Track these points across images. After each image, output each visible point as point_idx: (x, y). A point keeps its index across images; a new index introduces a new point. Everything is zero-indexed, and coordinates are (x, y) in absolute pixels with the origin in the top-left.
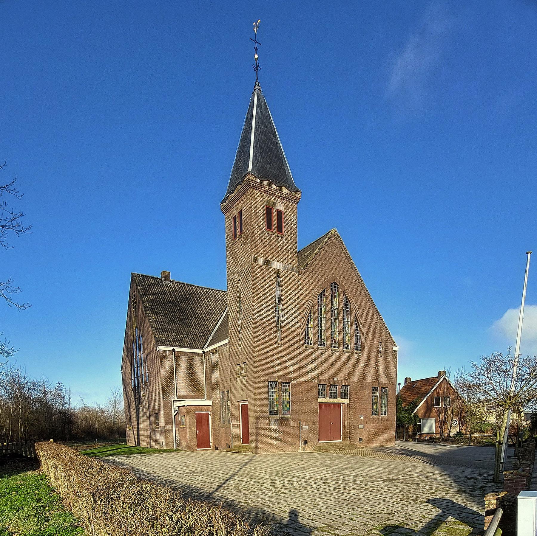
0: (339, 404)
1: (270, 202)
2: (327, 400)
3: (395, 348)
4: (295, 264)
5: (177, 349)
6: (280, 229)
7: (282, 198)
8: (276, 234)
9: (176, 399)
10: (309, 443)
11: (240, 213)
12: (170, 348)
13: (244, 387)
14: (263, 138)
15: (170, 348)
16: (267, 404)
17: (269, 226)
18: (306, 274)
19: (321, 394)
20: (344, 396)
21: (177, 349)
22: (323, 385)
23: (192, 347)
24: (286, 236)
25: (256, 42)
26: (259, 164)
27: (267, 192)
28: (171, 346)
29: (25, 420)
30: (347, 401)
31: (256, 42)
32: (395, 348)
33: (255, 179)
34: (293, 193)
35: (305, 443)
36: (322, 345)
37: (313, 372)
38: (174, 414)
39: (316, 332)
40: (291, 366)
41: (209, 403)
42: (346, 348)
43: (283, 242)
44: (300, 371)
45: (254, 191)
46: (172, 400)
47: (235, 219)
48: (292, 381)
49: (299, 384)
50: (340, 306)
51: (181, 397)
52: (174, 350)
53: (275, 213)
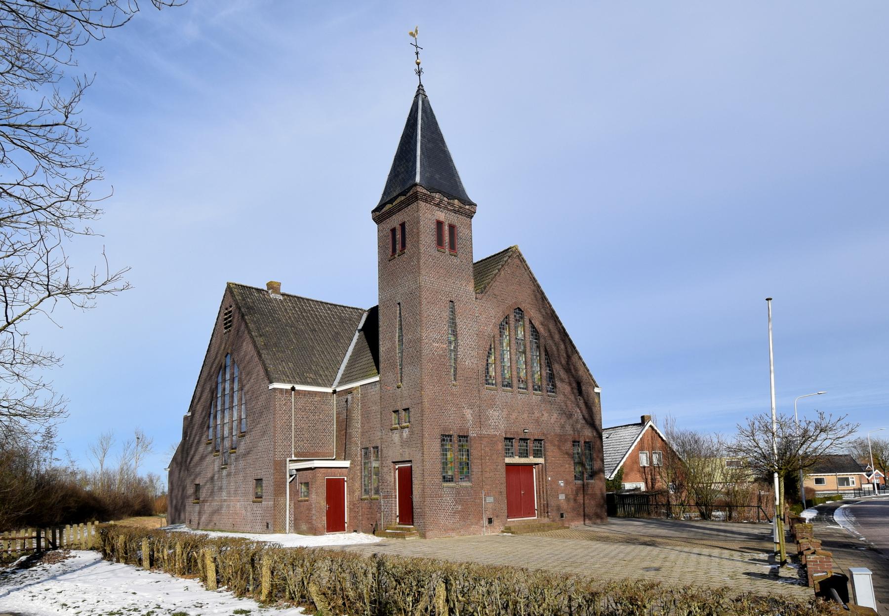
0: (530, 466)
1: (441, 215)
2: (517, 460)
3: (596, 390)
4: (471, 287)
5: (298, 387)
6: (452, 246)
7: (455, 212)
8: (447, 252)
9: (294, 458)
10: (496, 522)
11: (403, 225)
12: (288, 386)
13: (404, 443)
14: (430, 145)
15: (288, 386)
16: (439, 466)
17: (440, 242)
18: (484, 299)
19: (508, 452)
20: (537, 454)
21: (298, 387)
22: (510, 439)
23: (319, 385)
24: (459, 254)
25: (417, 47)
26: (428, 175)
27: (438, 205)
28: (290, 382)
29: (135, 491)
30: (541, 460)
31: (417, 47)
32: (596, 390)
33: (424, 191)
34: (467, 207)
35: (490, 521)
36: (507, 386)
37: (498, 422)
38: (289, 480)
39: (499, 369)
40: (468, 414)
41: (347, 464)
42: (536, 390)
43: (456, 261)
44: (480, 419)
45: (422, 204)
46: (288, 459)
47: (393, 231)
48: (472, 434)
49: (481, 437)
50: (527, 336)
51: (303, 456)
52: (293, 389)
53: (446, 228)
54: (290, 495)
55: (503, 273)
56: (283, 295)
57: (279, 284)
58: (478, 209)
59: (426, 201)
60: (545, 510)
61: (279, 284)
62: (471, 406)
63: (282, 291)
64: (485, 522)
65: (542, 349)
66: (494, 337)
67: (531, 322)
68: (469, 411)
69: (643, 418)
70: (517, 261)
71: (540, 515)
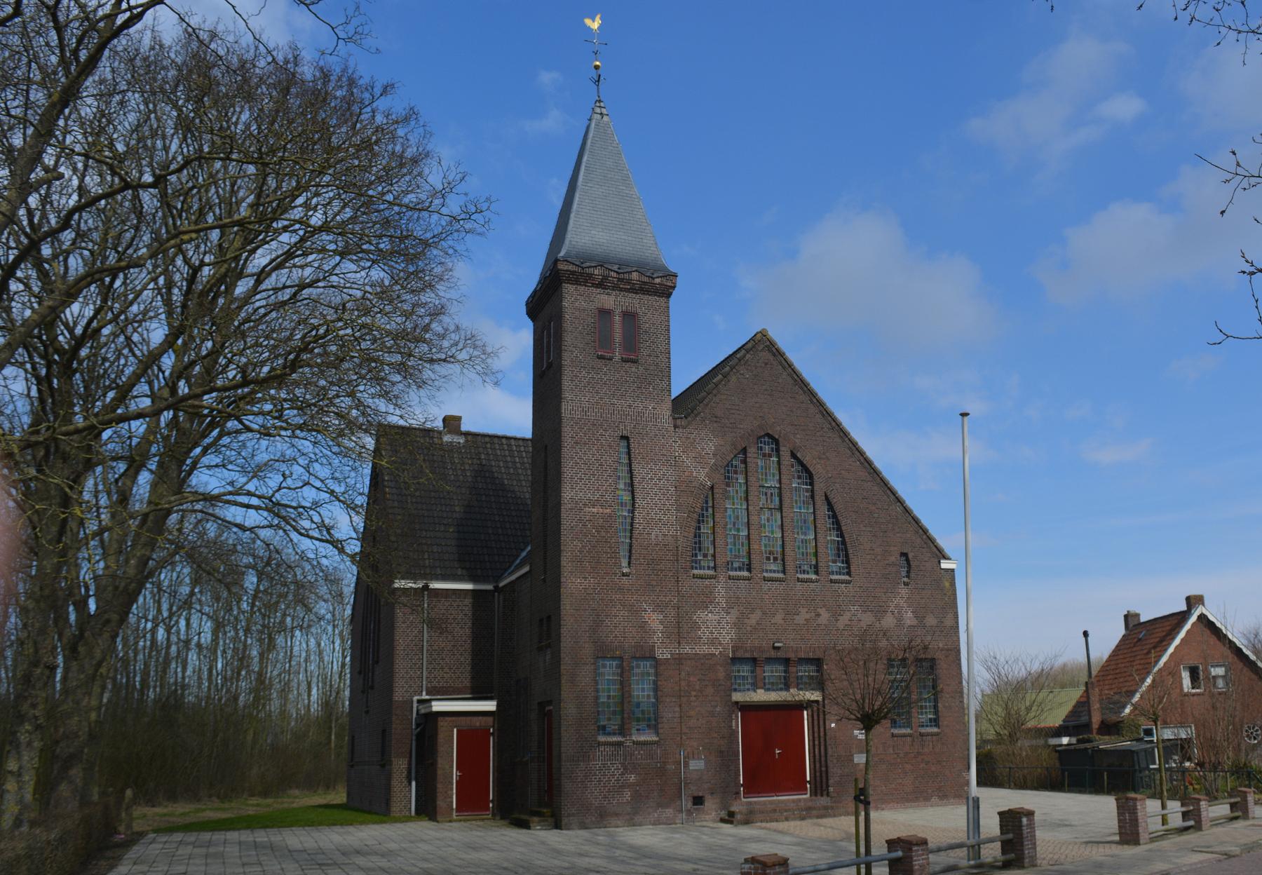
0: (799, 706)
40: (654, 620)
41: (490, 706)
44: (680, 629)
49: (679, 660)
54: (967, 741)
55: (733, 379)
56: (467, 434)
57: (459, 418)
58: (679, 281)
59: (577, 282)
60: (820, 787)
61: (459, 418)
62: (659, 608)
63: (464, 428)
64: (687, 803)
65: (820, 499)
66: (712, 488)
67: (793, 455)
68: (654, 616)
69: (1188, 599)
70: (766, 355)
71: (814, 793)
